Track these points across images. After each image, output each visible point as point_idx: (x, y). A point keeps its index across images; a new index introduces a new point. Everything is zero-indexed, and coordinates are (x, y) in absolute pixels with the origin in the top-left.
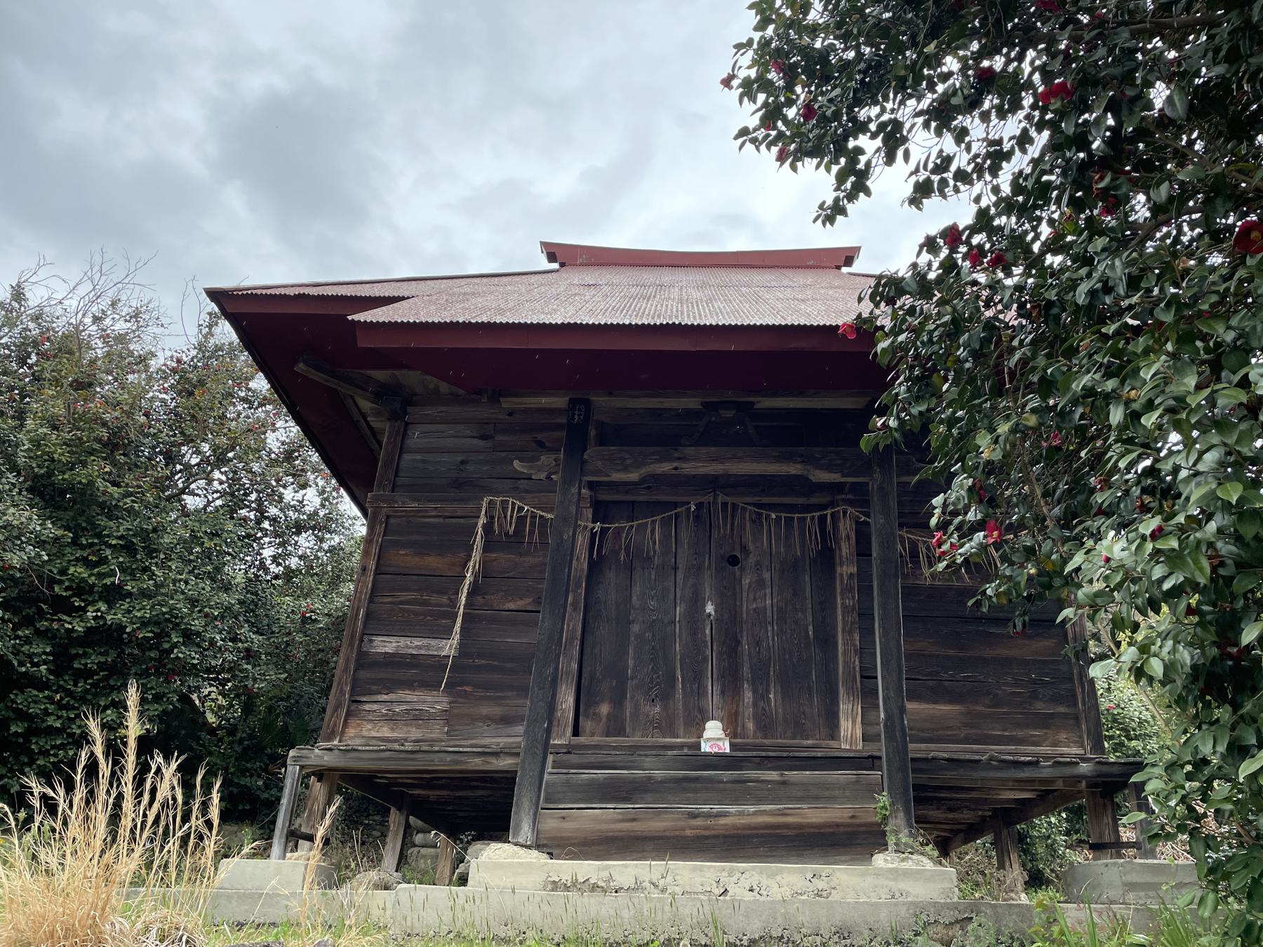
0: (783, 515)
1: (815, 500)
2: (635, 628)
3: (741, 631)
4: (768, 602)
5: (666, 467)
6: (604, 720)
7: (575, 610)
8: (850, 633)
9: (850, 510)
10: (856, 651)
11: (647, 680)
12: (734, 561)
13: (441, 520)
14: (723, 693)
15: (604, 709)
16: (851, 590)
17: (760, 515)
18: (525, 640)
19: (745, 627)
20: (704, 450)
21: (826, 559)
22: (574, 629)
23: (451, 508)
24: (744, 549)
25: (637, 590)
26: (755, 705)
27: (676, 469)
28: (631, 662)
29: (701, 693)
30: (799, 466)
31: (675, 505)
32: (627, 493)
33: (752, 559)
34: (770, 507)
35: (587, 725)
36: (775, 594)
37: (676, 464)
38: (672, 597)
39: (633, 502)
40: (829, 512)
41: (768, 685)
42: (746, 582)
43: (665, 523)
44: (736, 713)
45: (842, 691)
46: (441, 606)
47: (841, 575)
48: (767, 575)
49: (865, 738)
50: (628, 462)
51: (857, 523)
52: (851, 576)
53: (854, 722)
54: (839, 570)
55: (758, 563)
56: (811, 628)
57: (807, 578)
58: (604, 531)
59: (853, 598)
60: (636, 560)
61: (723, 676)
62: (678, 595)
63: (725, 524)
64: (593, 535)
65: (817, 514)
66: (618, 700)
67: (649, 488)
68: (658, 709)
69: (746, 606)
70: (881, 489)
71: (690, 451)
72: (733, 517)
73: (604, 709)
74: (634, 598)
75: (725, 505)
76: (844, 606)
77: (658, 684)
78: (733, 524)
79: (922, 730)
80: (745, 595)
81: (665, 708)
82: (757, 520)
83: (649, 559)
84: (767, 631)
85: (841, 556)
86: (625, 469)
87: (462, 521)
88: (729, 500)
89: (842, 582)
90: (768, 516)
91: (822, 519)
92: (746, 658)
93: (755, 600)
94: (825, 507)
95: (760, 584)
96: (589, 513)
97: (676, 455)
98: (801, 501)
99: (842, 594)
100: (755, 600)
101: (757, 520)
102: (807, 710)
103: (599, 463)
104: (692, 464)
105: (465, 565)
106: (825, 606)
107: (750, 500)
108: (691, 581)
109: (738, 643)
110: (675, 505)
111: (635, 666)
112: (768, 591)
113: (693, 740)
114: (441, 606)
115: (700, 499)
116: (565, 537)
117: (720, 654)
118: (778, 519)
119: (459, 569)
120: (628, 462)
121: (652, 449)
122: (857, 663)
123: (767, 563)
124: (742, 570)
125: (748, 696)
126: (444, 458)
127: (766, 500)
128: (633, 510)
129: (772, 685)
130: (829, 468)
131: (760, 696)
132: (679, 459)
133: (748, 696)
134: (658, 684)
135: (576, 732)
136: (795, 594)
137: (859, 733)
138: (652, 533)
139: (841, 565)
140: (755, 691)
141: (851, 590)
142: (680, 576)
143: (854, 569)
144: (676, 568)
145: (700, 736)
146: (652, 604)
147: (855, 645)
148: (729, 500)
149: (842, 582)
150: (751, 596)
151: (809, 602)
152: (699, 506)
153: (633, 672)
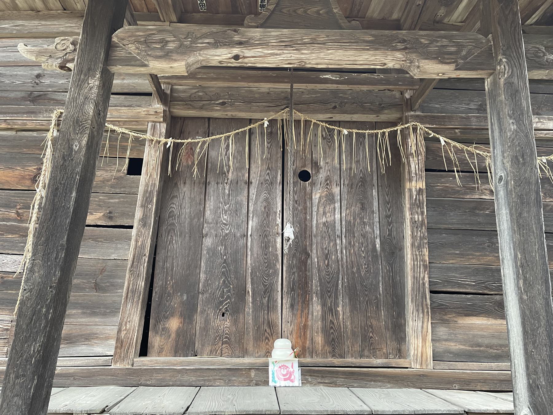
0: (355, 131)
1: (384, 117)
2: (208, 242)
3: (311, 245)
4: (338, 216)
5: (221, 56)
6: (173, 335)
7: (144, 225)
8: (419, 247)
9: (419, 126)
10: (425, 267)
11: (218, 293)
12: (304, 176)
13: (13, 133)
14: (292, 306)
15: (174, 324)
16: (420, 205)
17: (331, 131)
18: (92, 256)
19: (314, 240)
20: (275, 32)
21: (394, 175)
22: (143, 246)
23: (21, 120)
24: (316, 165)
25: (210, 205)
26: (324, 318)
27: (236, 57)
28: (202, 276)
29: (270, 307)
30: (399, 55)
31: (250, 121)
32: (201, 108)
33: (322, 175)
34: (339, 123)
35: (155, 340)
36: (344, 208)
37: (236, 51)
38: (245, 211)
39: (209, 119)
40: (399, 128)
41: (336, 298)
42: (316, 196)
43: (239, 138)
44: (305, 326)
45: (410, 306)
46: (9, 220)
47: (410, 190)
48: (336, 190)
49: (436, 358)
50: (171, 46)
51: (426, 139)
52: (420, 191)
53: (424, 340)
54: (408, 185)
55: (328, 179)
56: (378, 241)
57: (375, 193)
58: (177, 146)
59: (422, 213)
60: (210, 172)
61: (293, 289)
62: (251, 209)
63: (298, 141)
64: (166, 151)
65: (387, 131)
66: (189, 312)
67: (223, 104)
68: (228, 323)
69: (317, 220)
70: (509, 84)
71: (256, 33)
72: (305, 134)
73: (174, 324)
74: (208, 213)
75: (298, 122)
76: (413, 222)
77: (228, 297)
78: (305, 140)
79: (491, 347)
80: (315, 209)
81: (235, 322)
82: (328, 137)
83: (223, 174)
84: (336, 244)
85: (410, 172)
86: (167, 56)
87: (35, 134)
88: (302, 117)
89: (411, 196)
90: (339, 132)
91: (393, 135)
92: (315, 271)
93: (325, 213)
94: (395, 124)
95: (330, 198)
96: (163, 128)
97: (237, 38)
98: (371, 118)
99: (411, 209)
100: (325, 213)
101: (328, 137)
102: (374, 322)
103: (132, 48)
104: (259, 51)
105: (34, 179)
106: (392, 218)
107: (322, 117)
108: (263, 196)
109: (308, 255)
110: (250, 121)
111: (206, 280)
112: (337, 205)
113: (262, 360)
114: (9, 220)
115: (273, 116)
116: (76, 148)
117: (290, 267)
118: (350, 134)
119: (28, 183)
120: (171, 46)
121: (205, 29)
122: (427, 279)
123: (336, 178)
124: (313, 184)
125: (316, 308)
126: (20, 71)
127: (338, 117)
128: (209, 126)
129: (341, 298)
130: (440, 57)
131: (329, 310)
132: (240, 43)
133: (316, 308)
134: (228, 297)
135: (144, 351)
136: (363, 208)
137: (429, 352)
138: (225, 148)
139: (410, 180)
140: (324, 305)
141: (420, 205)
142: (253, 191)
143: (422, 185)
144: (249, 183)
145: (268, 354)
146: (225, 218)
147: (425, 261)
148: (302, 117)
149: (411, 196)
150: (321, 210)
151: (376, 215)
152: (272, 122)
153: (204, 286)
